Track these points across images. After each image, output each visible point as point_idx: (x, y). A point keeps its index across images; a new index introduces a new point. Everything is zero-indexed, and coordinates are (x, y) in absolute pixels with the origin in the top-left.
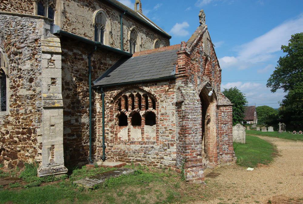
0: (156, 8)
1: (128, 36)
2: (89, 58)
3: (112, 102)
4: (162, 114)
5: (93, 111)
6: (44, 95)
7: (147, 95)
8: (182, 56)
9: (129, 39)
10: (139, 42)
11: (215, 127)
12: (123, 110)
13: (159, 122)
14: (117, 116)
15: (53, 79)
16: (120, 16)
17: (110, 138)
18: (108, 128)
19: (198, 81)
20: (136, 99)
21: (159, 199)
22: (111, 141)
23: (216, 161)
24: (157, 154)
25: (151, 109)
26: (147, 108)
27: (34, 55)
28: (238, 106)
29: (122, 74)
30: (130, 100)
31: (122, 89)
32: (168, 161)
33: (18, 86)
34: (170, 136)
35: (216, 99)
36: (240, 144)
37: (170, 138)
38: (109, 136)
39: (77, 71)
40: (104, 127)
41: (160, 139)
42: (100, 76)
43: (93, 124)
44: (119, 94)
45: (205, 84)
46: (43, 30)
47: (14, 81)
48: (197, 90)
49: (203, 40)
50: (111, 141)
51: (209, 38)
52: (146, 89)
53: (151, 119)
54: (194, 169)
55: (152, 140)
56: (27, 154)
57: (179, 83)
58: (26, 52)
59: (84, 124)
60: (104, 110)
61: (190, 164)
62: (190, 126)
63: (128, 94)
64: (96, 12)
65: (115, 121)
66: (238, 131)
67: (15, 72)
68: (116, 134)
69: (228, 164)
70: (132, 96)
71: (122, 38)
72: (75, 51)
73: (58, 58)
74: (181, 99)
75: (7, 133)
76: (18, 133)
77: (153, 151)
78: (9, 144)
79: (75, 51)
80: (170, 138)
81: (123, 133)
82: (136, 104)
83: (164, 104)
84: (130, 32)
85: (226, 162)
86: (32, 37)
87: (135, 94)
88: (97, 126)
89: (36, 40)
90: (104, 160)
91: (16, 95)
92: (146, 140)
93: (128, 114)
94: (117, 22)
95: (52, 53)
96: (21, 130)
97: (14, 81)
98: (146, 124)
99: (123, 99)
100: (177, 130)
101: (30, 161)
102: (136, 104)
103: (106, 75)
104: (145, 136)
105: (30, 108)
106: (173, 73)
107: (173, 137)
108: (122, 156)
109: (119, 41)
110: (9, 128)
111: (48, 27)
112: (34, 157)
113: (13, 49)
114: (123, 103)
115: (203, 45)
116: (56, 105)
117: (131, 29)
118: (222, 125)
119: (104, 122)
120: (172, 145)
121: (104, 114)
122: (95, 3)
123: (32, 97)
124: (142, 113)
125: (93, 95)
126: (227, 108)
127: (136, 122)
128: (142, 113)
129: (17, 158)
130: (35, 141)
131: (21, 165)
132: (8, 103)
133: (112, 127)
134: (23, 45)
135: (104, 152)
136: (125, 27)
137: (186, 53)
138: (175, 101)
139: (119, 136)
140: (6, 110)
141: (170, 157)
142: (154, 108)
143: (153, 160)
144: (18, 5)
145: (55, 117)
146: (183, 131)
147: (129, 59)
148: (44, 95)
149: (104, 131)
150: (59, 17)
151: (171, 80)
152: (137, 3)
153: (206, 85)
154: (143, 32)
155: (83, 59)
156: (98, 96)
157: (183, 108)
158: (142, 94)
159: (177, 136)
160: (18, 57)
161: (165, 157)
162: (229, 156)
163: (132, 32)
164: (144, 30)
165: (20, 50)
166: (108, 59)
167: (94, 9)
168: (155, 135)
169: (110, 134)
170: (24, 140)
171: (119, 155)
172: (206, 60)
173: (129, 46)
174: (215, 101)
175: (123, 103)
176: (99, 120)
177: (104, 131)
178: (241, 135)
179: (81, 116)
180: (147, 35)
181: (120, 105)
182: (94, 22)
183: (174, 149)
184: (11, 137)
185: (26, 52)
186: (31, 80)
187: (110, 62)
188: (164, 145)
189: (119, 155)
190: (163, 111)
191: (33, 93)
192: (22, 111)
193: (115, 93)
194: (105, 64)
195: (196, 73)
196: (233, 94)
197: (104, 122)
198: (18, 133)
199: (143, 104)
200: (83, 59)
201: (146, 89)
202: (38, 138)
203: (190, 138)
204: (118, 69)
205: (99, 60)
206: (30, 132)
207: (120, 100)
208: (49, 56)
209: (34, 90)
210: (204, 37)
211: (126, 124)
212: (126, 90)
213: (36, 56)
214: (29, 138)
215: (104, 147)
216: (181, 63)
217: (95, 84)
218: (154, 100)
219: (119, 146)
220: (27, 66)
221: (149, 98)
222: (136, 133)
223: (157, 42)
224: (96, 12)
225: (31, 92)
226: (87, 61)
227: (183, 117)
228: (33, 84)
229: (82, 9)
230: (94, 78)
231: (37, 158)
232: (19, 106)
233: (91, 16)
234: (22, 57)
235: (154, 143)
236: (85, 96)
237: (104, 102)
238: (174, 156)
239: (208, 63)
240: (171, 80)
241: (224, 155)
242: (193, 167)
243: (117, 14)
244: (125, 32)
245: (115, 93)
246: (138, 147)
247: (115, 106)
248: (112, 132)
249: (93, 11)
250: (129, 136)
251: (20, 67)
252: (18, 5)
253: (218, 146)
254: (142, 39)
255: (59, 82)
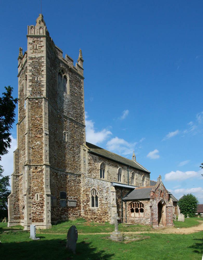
0: (141, 141)
1: (131, 175)
2: (121, 191)
3: (129, 205)
4: (146, 209)
5: (123, 207)
6: (112, 203)
7: (141, 203)
8: (152, 193)
9: (131, 177)
10: (135, 177)
11: (165, 214)
12: (133, 207)
13: (144, 211)
14: (131, 209)
15: (113, 199)
16: (128, 168)
17: (128, 216)
18: (128, 213)
19: (158, 199)
20: (137, 204)
21: (150, 181)
22: (129, 217)
23: (166, 225)
24: (144, 221)
25: (142, 208)
26: (141, 207)
27: (107, 192)
28: (193, 204)
29: (131, 196)
30: (135, 204)
31: (131, 202)
32: (147, 223)
33: (102, 200)
34: (148, 216)
35: (166, 204)
36: (182, 222)
37: (148, 216)
38: (128, 215)
39: (118, 196)
40: (126, 212)
41: (145, 216)
42: (124, 196)
43: (122, 211)
44: (131, 203)
45: (160, 200)
46: (110, 185)
47: (100, 199)
48: (157, 202)
49: (160, 186)
50: (129, 217)
51: (163, 185)
52: (140, 201)
53: (142, 211)
54: (155, 225)
55: (142, 217)
56: (105, 219)
57: (151, 200)
58: (105, 191)
59: (120, 211)
60: (126, 207)
61: (154, 224)
62: (154, 213)
63: (134, 203)
64: (119, 168)
65: (130, 211)
66: (181, 216)
67: (101, 196)
68: (130, 215)
69: (171, 227)
70: (136, 203)
71: (128, 177)
72: (118, 190)
73: (115, 193)
74: (151, 205)
75: (98, 213)
76: (102, 213)
77: (143, 220)
78: (99, 216)
79: (118, 190)
80: (148, 216)
81: (133, 214)
82: (137, 206)
83: (146, 206)
84: (131, 174)
85: (170, 226)
86: (107, 187)
87: (137, 203)
88: (124, 212)
89: (108, 188)
90: (126, 222)
91: (101, 203)
92: (140, 217)
93: (134, 209)
94: (126, 171)
95: (113, 192)
96: (103, 212)
97: (100, 199)
98: (140, 212)
99: (132, 204)
100: (150, 214)
101: (106, 221)
102: (137, 206)
103: (126, 196)
104: (140, 216)
105: (106, 206)
106: (149, 197)
107: (149, 216)
108: (133, 221)
109: (127, 178)
110: (99, 212)
111: (111, 184)
112: (107, 220)
113: (100, 190)
114: (132, 205)
115: (160, 187)
116: (115, 206)
117: (132, 172)
118: (169, 213)
119: (126, 211)
120: (149, 218)
121: (126, 209)
122: (118, 165)
123: (107, 203)
124: (139, 209)
125: (122, 203)
126: (171, 207)
127: (137, 211)
128: (139, 209)
129: (102, 220)
130: (108, 215)
131: (103, 222)
132: (99, 205)
133: (129, 213)
134: (103, 189)
135: (126, 220)
136: (129, 172)
137: (153, 192)
138: (150, 206)
139: (131, 215)
140: (98, 207)
141: (148, 222)
142: (143, 207)
143: (142, 223)
144: (95, 172)
145: (115, 209)
146: (152, 214)
147: (115, 160)
148: (112, 203)
149: (126, 214)
150: (106, 173)
151: (148, 199)
152: (134, 157)
153: (161, 200)
154: (137, 173)
155: (119, 192)
156: (124, 203)
157: (152, 208)
158: (139, 203)
159: (150, 216)
160: (102, 192)
161: (147, 222)
162: (171, 224)
163: (132, 173)
164: (138, 172)
165: (103, 190)
166: (127, 191)
167: (118, 167)
168: (143, 215)
169: (128, 215)
170: (104, 215)
171: (131, 221)
172: (162, 192)
173: (131, 180)
174: (165, 205)
175: (132, 205)
176: (124, 210)
177: (126, 214)
178: (182, 218)
179: (119, 209)
180: (139, 173)
181: (131, 206)
182: (118, 173)
183: (149, 219)
184: (100, 214)
185: (105, 191)
186: (106, 199)
187: (127, 191)
188: (146, 218)
189: (131, 221)
190: (146, 208)
191: (107, 202)
192: (103, 207)
193: (130, 202)
194: (126, 192)
195: (157, 197)
196: (189, 198)
197: (126, 211)
198: (102, 213)
199: (139, 206)
200: (119, 192)
201: (140, 201)
202: (109, 215)
203: (154, 216)
204: (130, 194)
205: (124, 191)
206: (106, 213)
207: (132, 204)
208: (112, 193)
209: (107, 202)
210: (160, 184)
211: (133, 212)
212: (134, 201)
213: (108, 192)
214: (106, 215)
215: (126, 219)
216: (152, 195)
217: (123, 199)
218: (143, 205)
219: (131, 218)
220: (105, 195)
221: (141, 204)
222: (137, 215)
223: (143, 176)
224: (119, 168)
225: (107, 202)
226: (121, 192)
227: (152, 211)
228: (107, 200)
229: (113, 169)
230: (123, 197)
231: (109, 220)
232: (103, 206)
233: (117, 171)
234: (103, 192)
235: (143, 218)
236: (120, 203)
237: (126, 205)
238: (150, 222)
239: (162, 193)
240: (148, 199)
241: (169, 224)
242: (155, 224)
243: (126, 167)
244: (130, 174)
245: (130, 202)
246: (138, 219)
247: (130, 206)
248: (129, 214)
249: (117, 168)
250: (135, 215)
251: (102, 195)
252: (95, 172)
253: (167, 220)
254: (137, 176)
255: (115, 200)
